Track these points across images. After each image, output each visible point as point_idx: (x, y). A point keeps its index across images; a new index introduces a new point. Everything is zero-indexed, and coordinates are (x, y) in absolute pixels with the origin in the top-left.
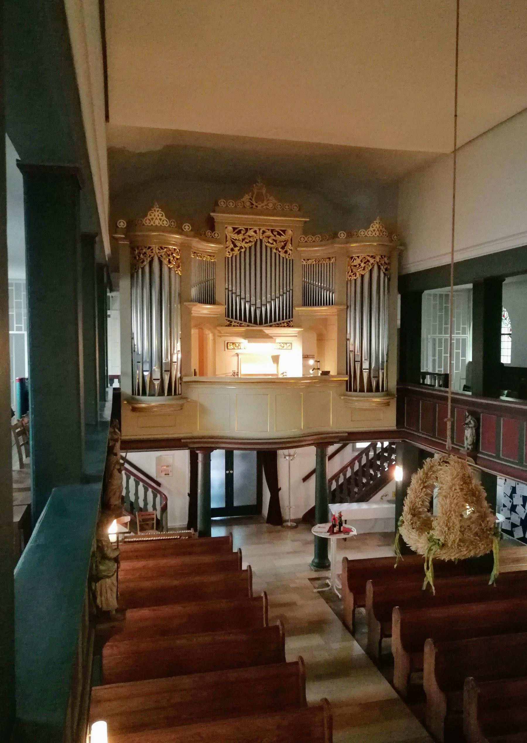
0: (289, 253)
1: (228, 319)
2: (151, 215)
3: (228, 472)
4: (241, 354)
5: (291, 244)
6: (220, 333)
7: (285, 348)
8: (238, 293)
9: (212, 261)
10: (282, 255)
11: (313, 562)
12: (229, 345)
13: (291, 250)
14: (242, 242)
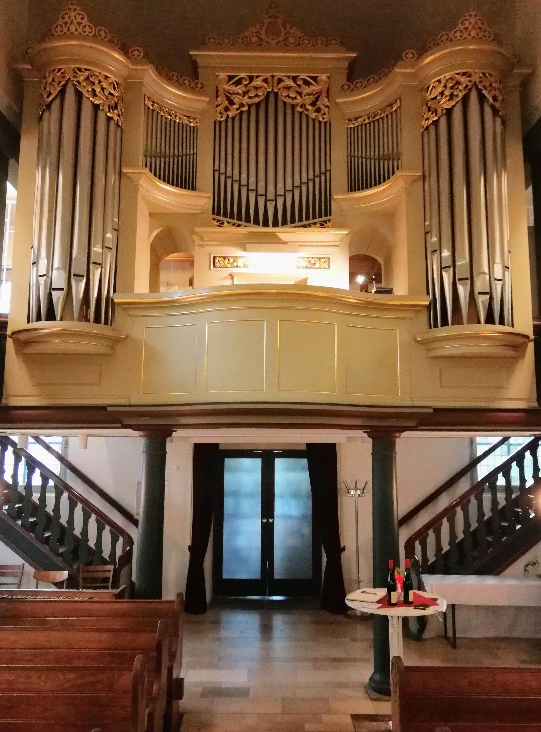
0: (323, 112)
1: (218, 218)
2: (63, 18)
3: (265, 520)
4: (239, 274)
5: (328, 97)
6: (202, 239)
7: (317, 265)
8: (236, 177)
9: (192, 125)
10: (313, 115)
11: (371, 679)
12: (217, 260)
13: (327, 107)
14: (244, 97)
